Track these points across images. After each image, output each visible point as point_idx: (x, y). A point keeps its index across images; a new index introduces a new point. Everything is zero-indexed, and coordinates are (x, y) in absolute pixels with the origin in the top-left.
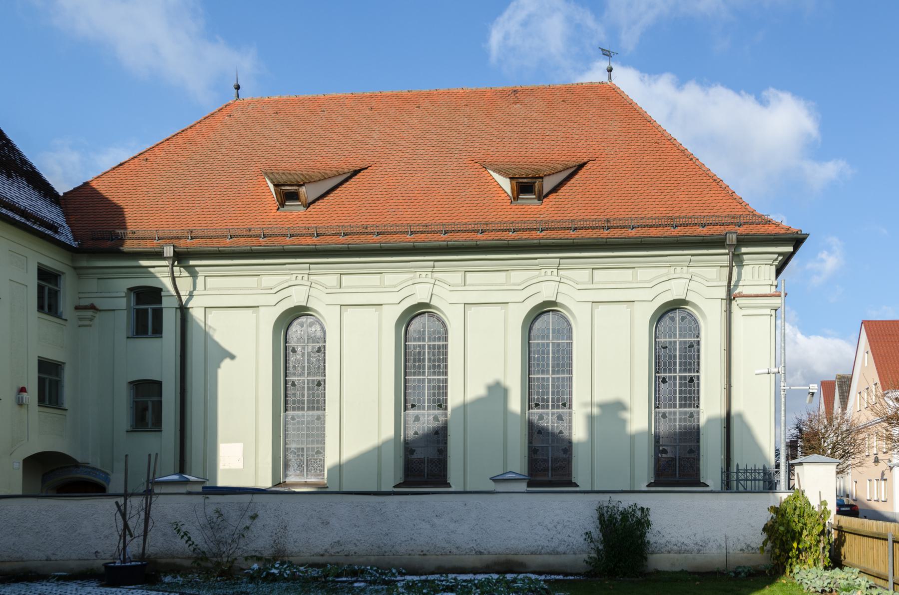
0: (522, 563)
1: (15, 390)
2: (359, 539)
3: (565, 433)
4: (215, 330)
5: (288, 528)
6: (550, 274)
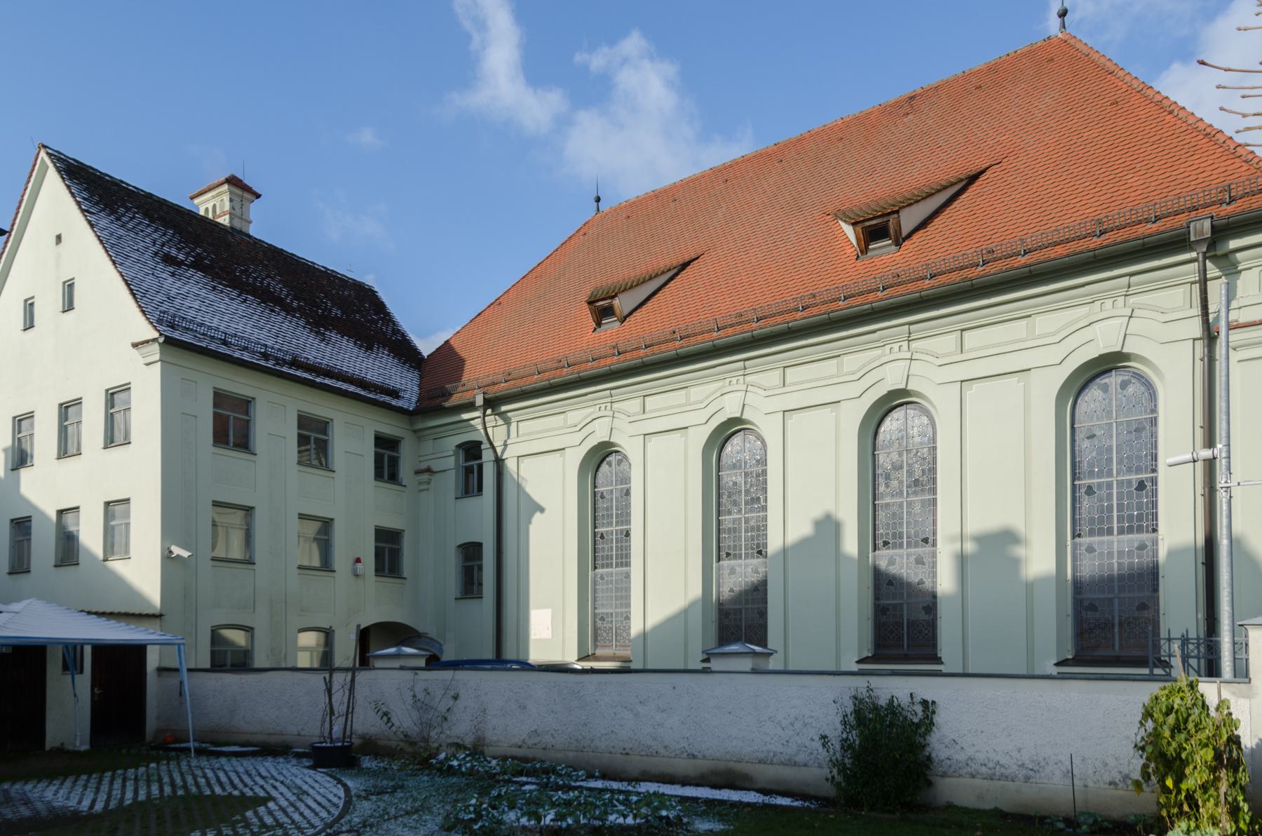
0: (747, 774)
1: (351, 561)
2: (556, 728)
3: (927, 583)
4: (526, 481)
5: (487, 711)
6: (899, 350)
